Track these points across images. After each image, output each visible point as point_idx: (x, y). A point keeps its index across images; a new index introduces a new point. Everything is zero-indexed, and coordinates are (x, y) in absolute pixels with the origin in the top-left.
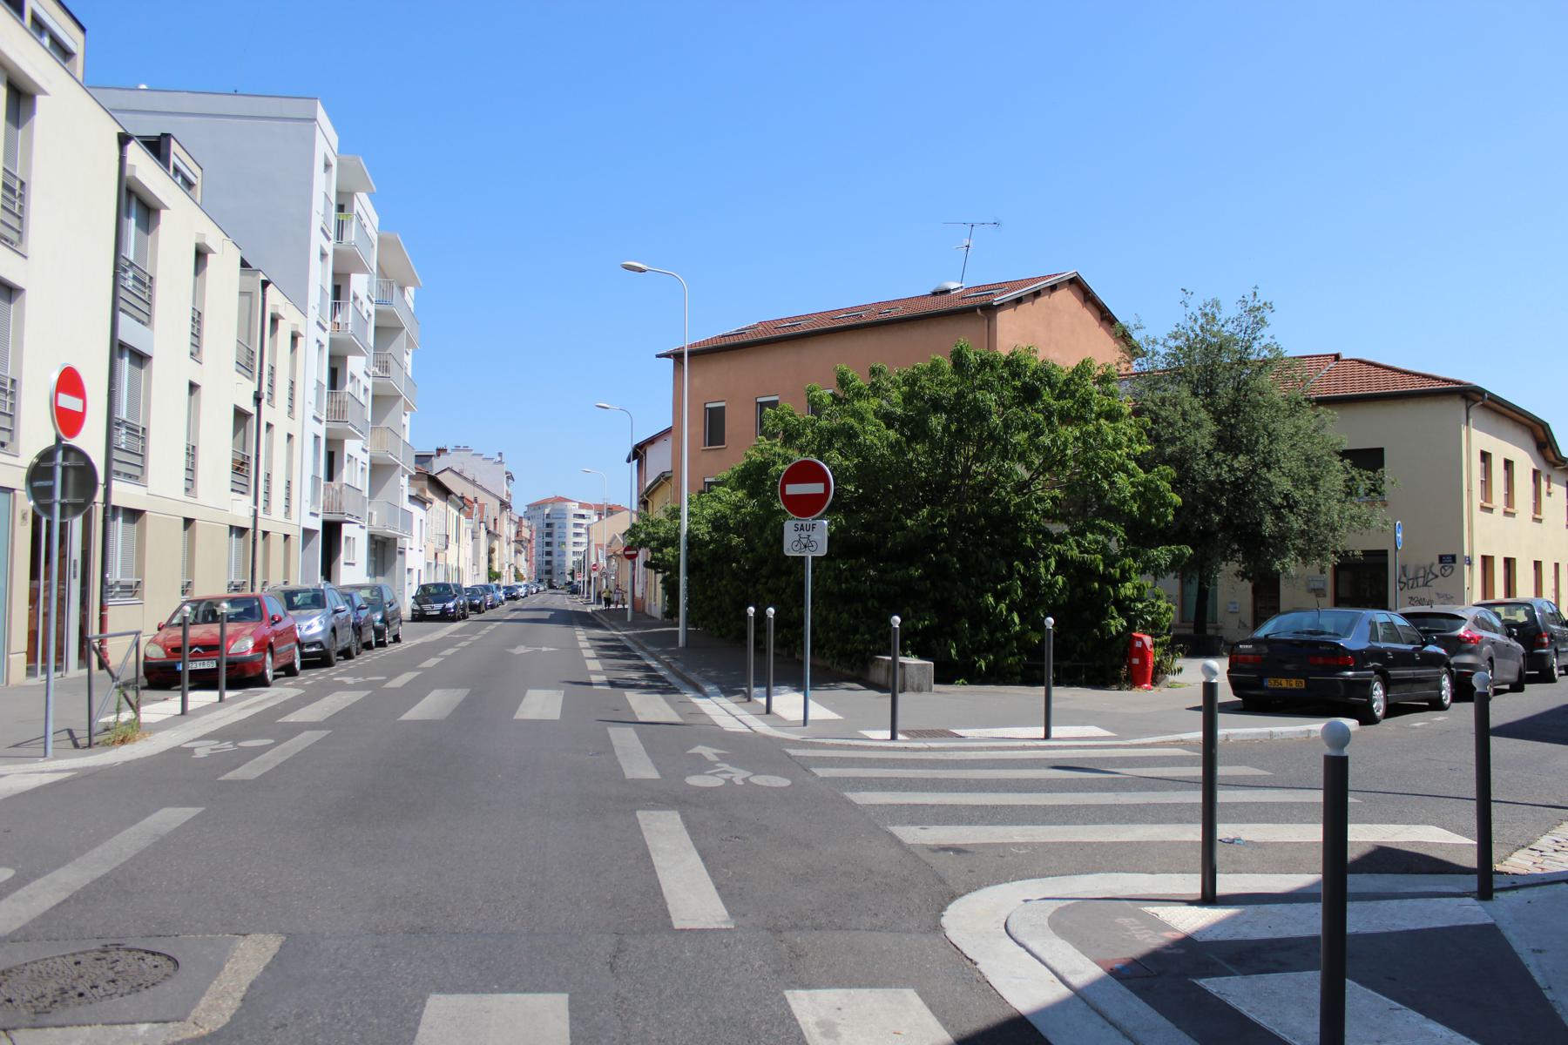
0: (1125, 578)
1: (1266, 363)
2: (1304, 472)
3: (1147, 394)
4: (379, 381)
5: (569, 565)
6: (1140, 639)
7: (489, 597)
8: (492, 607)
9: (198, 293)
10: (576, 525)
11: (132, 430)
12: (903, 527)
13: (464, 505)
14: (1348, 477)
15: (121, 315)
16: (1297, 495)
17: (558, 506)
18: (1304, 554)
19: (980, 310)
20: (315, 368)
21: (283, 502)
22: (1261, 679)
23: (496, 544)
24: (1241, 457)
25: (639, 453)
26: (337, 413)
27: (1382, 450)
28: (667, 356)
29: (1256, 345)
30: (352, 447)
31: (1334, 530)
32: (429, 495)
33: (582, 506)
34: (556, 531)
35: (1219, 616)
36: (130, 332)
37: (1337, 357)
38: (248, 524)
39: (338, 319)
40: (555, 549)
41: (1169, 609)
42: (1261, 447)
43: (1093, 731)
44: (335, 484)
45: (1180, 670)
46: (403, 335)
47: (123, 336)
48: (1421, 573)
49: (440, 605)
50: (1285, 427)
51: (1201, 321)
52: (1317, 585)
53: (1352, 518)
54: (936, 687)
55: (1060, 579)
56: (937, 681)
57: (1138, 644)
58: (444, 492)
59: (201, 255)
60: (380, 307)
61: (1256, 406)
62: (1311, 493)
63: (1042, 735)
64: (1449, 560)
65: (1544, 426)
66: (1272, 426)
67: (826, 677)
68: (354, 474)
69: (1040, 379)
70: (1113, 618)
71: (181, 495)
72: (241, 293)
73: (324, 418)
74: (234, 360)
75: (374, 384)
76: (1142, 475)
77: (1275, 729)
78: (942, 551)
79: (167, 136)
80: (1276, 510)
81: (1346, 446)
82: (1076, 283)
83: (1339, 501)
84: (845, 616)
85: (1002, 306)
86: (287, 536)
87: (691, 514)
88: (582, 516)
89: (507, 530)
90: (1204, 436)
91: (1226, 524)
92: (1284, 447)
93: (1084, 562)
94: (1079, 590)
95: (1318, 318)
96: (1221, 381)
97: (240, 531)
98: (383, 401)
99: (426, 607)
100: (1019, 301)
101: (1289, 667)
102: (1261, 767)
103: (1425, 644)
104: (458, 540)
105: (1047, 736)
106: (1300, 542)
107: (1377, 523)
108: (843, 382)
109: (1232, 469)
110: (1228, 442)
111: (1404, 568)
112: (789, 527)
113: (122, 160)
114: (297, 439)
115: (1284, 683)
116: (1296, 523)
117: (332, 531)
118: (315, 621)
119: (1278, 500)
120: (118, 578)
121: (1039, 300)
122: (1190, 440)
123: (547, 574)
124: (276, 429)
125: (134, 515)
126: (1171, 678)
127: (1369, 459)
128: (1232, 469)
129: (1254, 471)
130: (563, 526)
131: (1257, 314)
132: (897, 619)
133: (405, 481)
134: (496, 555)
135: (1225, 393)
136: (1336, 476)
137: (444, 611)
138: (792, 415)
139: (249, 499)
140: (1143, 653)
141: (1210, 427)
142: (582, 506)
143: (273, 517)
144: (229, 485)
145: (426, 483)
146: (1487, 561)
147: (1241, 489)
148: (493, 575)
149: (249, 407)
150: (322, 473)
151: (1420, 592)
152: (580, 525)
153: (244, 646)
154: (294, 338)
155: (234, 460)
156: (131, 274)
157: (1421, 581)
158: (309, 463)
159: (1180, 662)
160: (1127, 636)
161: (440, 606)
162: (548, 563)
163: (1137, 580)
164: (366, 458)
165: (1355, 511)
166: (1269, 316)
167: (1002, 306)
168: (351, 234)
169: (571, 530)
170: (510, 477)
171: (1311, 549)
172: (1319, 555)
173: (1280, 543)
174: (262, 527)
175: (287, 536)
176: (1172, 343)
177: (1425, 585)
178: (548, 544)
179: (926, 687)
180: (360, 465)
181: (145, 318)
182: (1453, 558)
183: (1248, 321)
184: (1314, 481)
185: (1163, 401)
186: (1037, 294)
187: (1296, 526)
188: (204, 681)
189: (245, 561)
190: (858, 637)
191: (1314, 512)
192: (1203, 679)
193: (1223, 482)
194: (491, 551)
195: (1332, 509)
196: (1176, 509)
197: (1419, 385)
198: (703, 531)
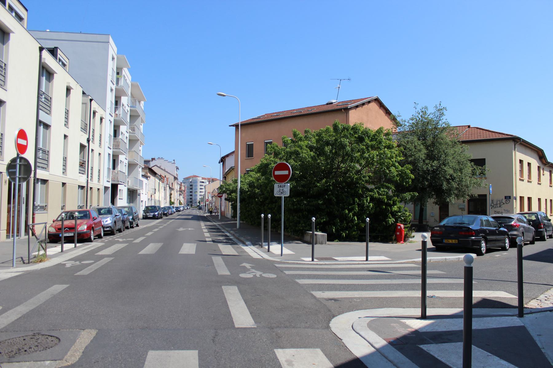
0: (394, 204)
2: (457, 167)
4: (131, 134)
5: (198, 199)
6: (400, 226)
7: (170, 211)
8: (171, 214)
9: (67, 103)
10: (201, 185)
12: (316, 186)
13: (161, 178)
16: (455, 175)
17: (194, 178)
18: (457, 196)
20: (109, 130)
21: (97, 177)
22: (442, 240)
23: (173, 192)
24: (435, 162)
25: (223, 160)
26: (116, 146)
27: (485, 159)
28: (233, 126)
29: (440, 122)
30: (122, 158)
31: (467, 187)
32: (149, 175)
33: (203, 178)
36: (43, 117)
38: (85, 185)
39: (117, 112)
41: (410, 215)
42: (442, 158)
44: (116, 171)
45: (414, 237)
48: (499, 202)
49: (152, 213)
50: (451, 151)
51: (421, 114)
52: (462, 207)
53: (474, 183)
54: (328, 243)
56: (328, 241)
57: (399, 227)
58: (154, 174)
59: (68, 90)
60: (132, 109)
61: (440, 144)
66: (446, 151)
67: (289, 239)
68: (122, 167)
70: (390, 218)
72: (83, 103)
73: (112, 147)
75: (129, 136)
77: (447, 257)
80: (448, 180)
81: (472, 158)
82: (377, 100)
83: (470, 177)
84: (296, 217)
85: (351, 108)
86: (98, 189)
87: (241, 182)
88: (203, 182)
89: (176, 187)
90: (422, 154)
91: (430, 185)
92: (451, 158)
93: (380, 199)
96: (428, 134)
97: (82, 187)
98: (133, 141)
99: (148, 214)
100: (357, 107)
103: (500, 227)
104: (159, 191)
105: (367, 260)
106: (456, 192)
107: (483, 185)
108: (295, 135)
109: (432, 166)
110: (431, 156)
111: (492, 201)
112: (276, 186)
113: (40, 56)
115: (450, 241)
116: (455, 185)
117: (114, 187)
118: (108, 219)
119: (448, 177)
120: (39, 204)
122: (417, 155)
123: (190, 202)
124: (95, 151)
125: (44, 182)
126: (410, 239)
127: (480, 162)
128: (432, 166)
129: (440, 167)
130: (196, 186)
131: (441, 111)
132: (314, 218)
135: (430, 139)
136: (469, 168)
137: (154, 215)
138: (277, 147)
139: (85, 176)
140: (400, 230)
141: (424, 151)
142: (203, 178)
144: (78, 171)
146: (522, 198)
147: (435, 173)
148: (171, 203)
149: (85, 143)
150: (111, 167)
151: (498, 209)
152: (202, 185)
153: (83, 228)
154: (101, 119)
155: (80, 162)
157: (498, 205)
158: (106, 163)
159: (414, 234)
160: (395, 225)
162: (191, 199)
163: (399, 205)
164: (127, 162)
166: (445, 112)
167: (351, 108)
168: (122, 83)
169: (199, 187)
170: (177, 168)
173: (449, 192)
174: (90, 186)
175: (98, 189)
176: (411, 122)
177: (500, 207)
178: (191, 192)
180: (124, 164)
181: (48, 112)
182: (510, 197)
183: (438, 114)
184: (461, 170)
188: (69, 240)
193: (429, 171)
194: (171, 194)
195: (467, 180)
196: (412, 180)
197: (498, 137)
198: (246, 187)
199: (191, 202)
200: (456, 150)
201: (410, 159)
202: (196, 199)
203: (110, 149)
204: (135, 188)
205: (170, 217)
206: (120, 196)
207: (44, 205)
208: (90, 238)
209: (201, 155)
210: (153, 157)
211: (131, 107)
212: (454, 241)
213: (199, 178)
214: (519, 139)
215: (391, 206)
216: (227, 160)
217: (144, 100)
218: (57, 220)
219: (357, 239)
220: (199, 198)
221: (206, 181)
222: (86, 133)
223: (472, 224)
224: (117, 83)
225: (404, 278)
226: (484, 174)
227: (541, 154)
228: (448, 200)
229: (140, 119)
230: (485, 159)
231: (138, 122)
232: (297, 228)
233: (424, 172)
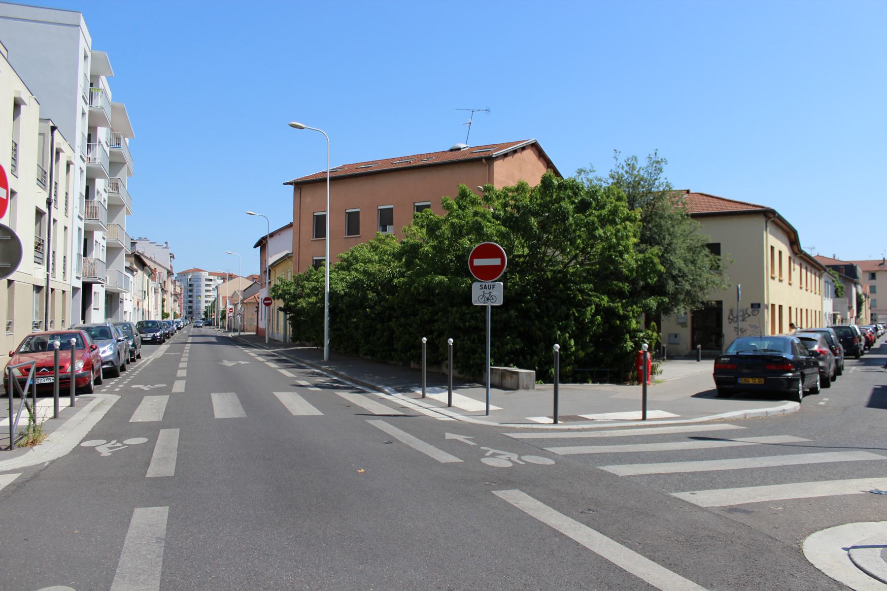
1: (664, 193)
5: (203, 309)
9: (16, 131)
10: (207, 285)
13: (152, 274)
16: (686, 270)
17: (196, 274)
19: (484, 160)
20: (78, 186)
21: (62, 270)
22: (736, 378)
23: (165, 297)
25: (262, 244)
26: (91, 214)
28: (290, 183)
29: (657, 183)
30: (98, 236)
32: (135, 267)
33: (210, 274)
34: (195, 289)
37: (688, 192)
38: (44, 284)
40: (194, 299)
44: (89, 258)
48: (741, 314)
49: (151, 333)
50: (678, 230)
51: (626, 168)
52: (681, 321)
54: (537, 386)
59: (17, 105)
62: (693, 268)
63: (641, 417)
64: (756, 307)
65: (795, 232)
66: (672, 229)
67: (460, 382)
68: (98, 253)
72: (40, 134)
73: (83, 217)
74: (36, 177)
77: (769, 410)
80: (674, 278)
82: (535, 146)
85: (497, 158)
86: (64, 292)
87: (330, 278)
88: (211, 280)
94: (607, 325)
95: (698, 171)
97: (38, 288)
98: (114, 208)
100: (505, 155)
101: (745, 371)
102: (803, 437)
105: (644, 418)
108: (463, 195)
111: (731, 311)
112: (476, 286)
114: (69, 230)
115: (751, 381)
117: (87, 288)
123: (190, 313)
124: (58, 222)
127: (715, 248)
130: (200, 286)
131: (657, 165)
132: (451, 340)
134: (165, 303)
139: (44, 268)
142: (210, 274)
143: (57, 279)
144: (33, 259)
145: (133, 259)
146: (773, 306)
148: (165, 315)
149: (44, 208)
150: (82, 253)
152: (209, 285)
154: (68, 165)
155: (36, 243)
157: (740, 318)
158: (76, 247)
161: (152, 335)
164: (104, 243)
167: (497, 158)
169: (204, 288)
170: (172, 257)
174: (51, 286)
175: (64, 292)
177: (743, 320)
178: (190, 296)
179: (531, 386)
182: (759, 305)
184: (693, 262)
186: (515, 152)
188: (45, 391)
189: (41, 308)
190: (477, 355)
197: (740, 208)
198: (340, 288)
199: (190, 313)
202: (198, 308)
203: (81, 219)
208: (89, 385)
209: (223, 232)
212: (757, 381)
213: (203, 273)
214: (773, 212)
216: (271, 244)
217: (129, 134)
218: (18, 352)
219: (571, 379)
220: (203, 307)
221: (216, 278)
222: (45, 189)
224: (91, 103)
227: (793, 237)
229: (125, 168)
231: (122, 174)
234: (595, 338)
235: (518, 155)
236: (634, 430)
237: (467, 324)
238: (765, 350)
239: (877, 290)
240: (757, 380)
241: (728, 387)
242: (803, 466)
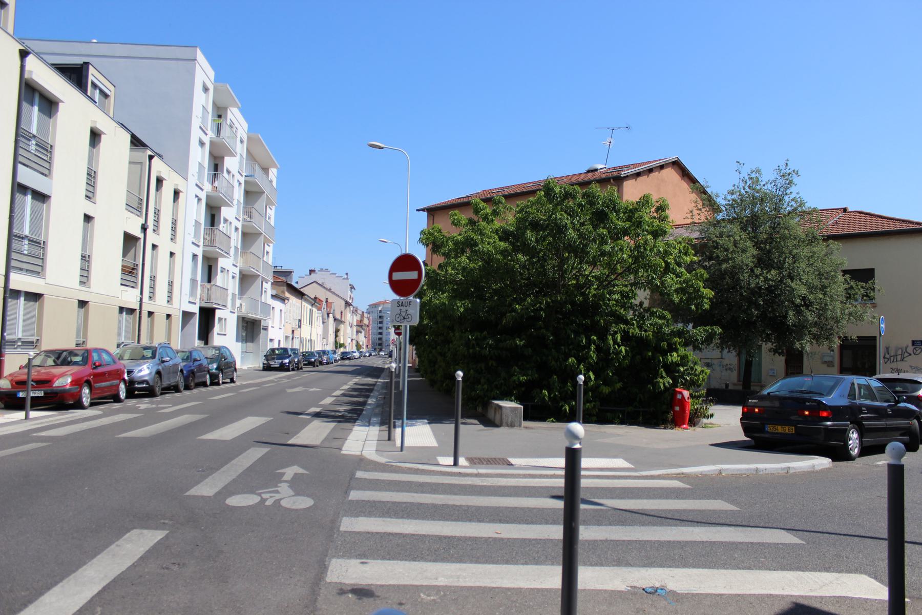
0: (672, 348)
2: (817, 283)
3: (712, 229)
4: (246, 223)
6: (681, 393)
7: (325, 358)
8: (327, 363)
11: (34, 242)
12: (515, 310)
13: (315, 302)
14: (847, 286)
15: (20, 166)
16: (811, 298)
18: (817, 338)
19: (616, 179)
21: (166, 294)
23: (342, 327)
24: (773, 272)
27: (873, 270)
28: (423, 210)
29: (786, 199)
31: (837, 322)
32: (287, 295)
35: (763, 378)
36: (27, 177)
39: (216, 184)
41: (702, 371)
42: (787, 265)
43: (620, 463)
45: (712, 416)
46: (264, 197)
47: (20, 179)
48: (900, 352)
50: (805, 252)
52: (827, 359)
53: (850, 314)
55: (623, 348)
56: (525, 419)
57: (679, 397)
58: (299, 294)
59: (95, 136)
60: (248, 179)
61: (784, 238)
69: (608, 207)
70: (662, 377)
71: (76, 284)
72: (130, 163)
73: (201, 244)
75: (243, 226)
76: (687, 275)
77: (760, 466)
78: (540, 328)
79: (87, 64)
81: (847, 267)
82: (677, 164)
83: (842, 302)
84: (472, 371)
85: (627, 178)
86: (168, 316)
89: (350, 318)
90: (748, 256)
91: (763, 316)
92: (803, 265)
93: (641, 337)
96: (763, 223)
97: (131, 311)
99: (271, 362)
100: (638, 175)
103: (897, 402)
104: (311, 323)
106: (814, 330)
107: (867, 317)
109: (766, 279)
110: (764, 261)
111: (887, 348)
113: (22, 67)
114: (178, 257)
115: (780, 429)
116: (810, 317)
118: (145, 367)
119: (798, 301)
120: (20, 336)
121: (652, 175)
122: (738, 259)
124: (160, 249)
125: (34, 297)
126: (705, 421)
127: (865, 275)
128: (766, 279)
129: (781, 281)
131: (787, 178)
133: (268, 286)
135: (764, 230)
136: (839, 286)
137: (282, 365)
138: (440, 231)
140: (682, 402)
141: (753, 251)
144: (119, 282)
145: (285, 288)
147: (773, 293)
148: (338, 345)
149: (138, 233)
151: (900, 365)
153: (64, 381)
154: (176, 193)
156: (34, 142)
157: (899, 358)
159: (714, 409)
160: (671, 392)
162: (380, 339)
163: (682, 351)
164: (237, 271)
165: (852, 309)
166: (796, 180)
167: (627, 178)
168: (226, 132)
170: (352, 288)
171: (823, 333)
172: (827, 339)
173: (800, 329)
174: (146, 308)
175: (168, 316)
176: (729, 197)
177: (902, 360)
178: (380, 328)
180: (231, 275)
181: (46, 172)
183: (781, 182)
184: (823, 288)
185: (721, 235)
187: (811, 319)
188: (37, 404)
191: (824, 309)
192: (567, 444)
193: (760, 288)
194: (337, 331)
195: (836, 308)
196: (710, 299)
199: (380, 344)
200: (815, 249)
201: (724, 266)
203: (198, 246)
204: (258, 317)
205: (321, 368)
206: (221, 330)
207: (35, 338)
210: (312, 268)
211: (246, 176)
215: (665, 353)
219: (594, 418)
223: (829, 393)
225: (623, 523)
226: (872, 299)
228: (797, 345)
230: (873, 270)
231: (261, 203)
232: (473, 394)
233: (753, 292)
234: (619, 372)
235: (654, 175)
236: (537, 480)
237: (471, 351)
238: (802, 392)
239: (286, 268)
240: (787, 428)
241: (759, 437)
242: (630, 542)
